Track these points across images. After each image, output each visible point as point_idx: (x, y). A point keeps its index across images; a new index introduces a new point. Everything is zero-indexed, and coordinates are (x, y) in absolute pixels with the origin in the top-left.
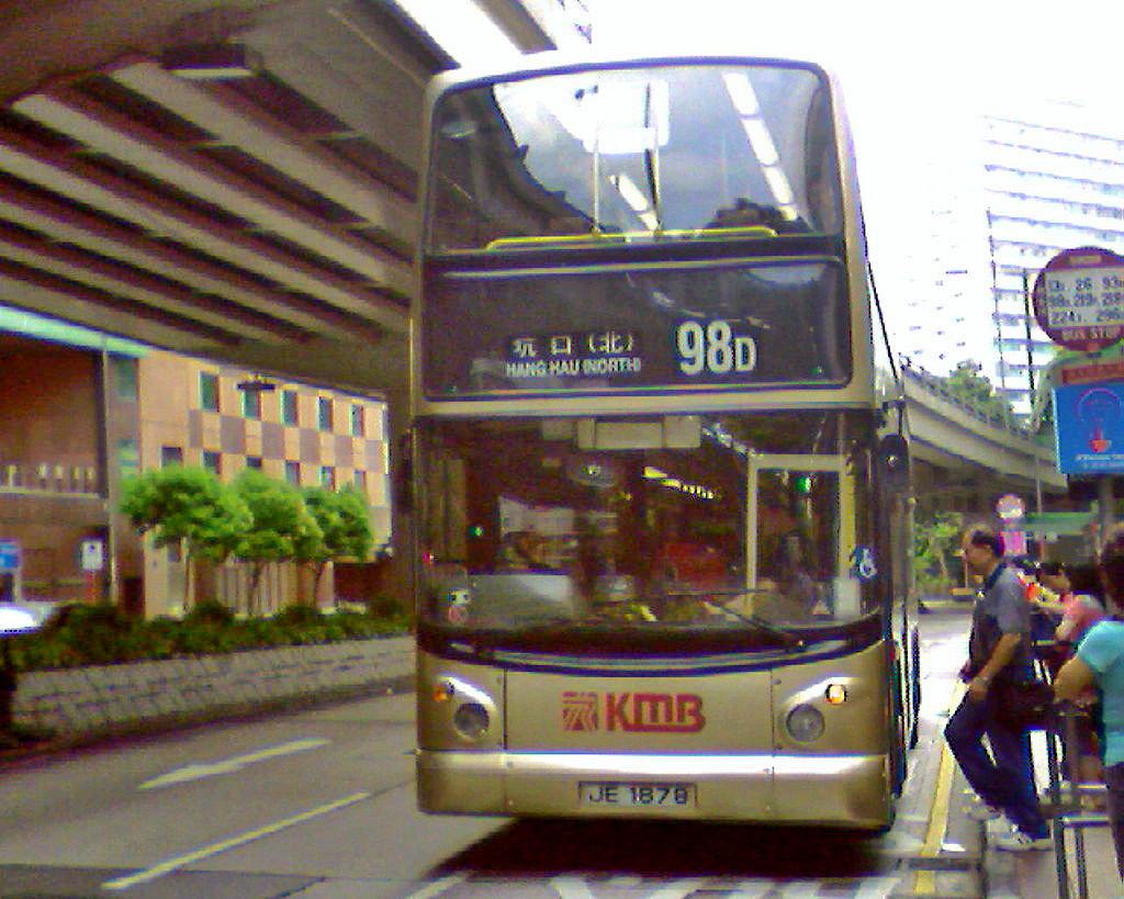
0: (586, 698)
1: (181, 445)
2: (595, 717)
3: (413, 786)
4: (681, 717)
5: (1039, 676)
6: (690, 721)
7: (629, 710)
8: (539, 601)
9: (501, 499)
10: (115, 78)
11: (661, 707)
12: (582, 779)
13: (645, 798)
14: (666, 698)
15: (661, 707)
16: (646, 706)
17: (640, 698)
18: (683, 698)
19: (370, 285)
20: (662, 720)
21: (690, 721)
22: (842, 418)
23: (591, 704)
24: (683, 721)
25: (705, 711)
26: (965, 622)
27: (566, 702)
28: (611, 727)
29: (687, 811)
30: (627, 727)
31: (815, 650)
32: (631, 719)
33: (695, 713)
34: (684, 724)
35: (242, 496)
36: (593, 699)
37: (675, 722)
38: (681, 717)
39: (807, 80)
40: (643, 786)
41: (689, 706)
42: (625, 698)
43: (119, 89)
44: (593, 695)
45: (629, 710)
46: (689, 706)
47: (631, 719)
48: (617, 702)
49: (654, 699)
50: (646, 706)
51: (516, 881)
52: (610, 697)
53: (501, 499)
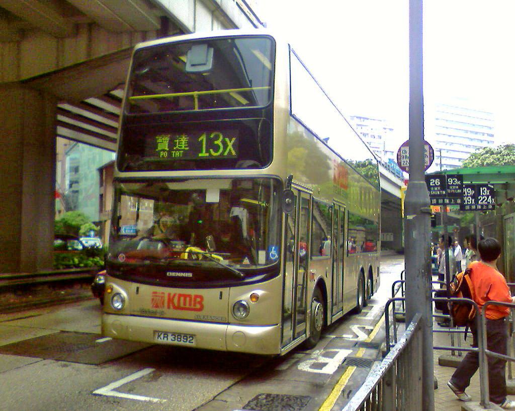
0: (160, 295)
1: (439, 366)
2: (163, 303)
4: (195, 305)
5: (293, 251)
6: (198, 306)
8: (333, 335)
12: (155, 329)
13: (179, 340)
14: (189, 296)
15: (188, 299)
16: (182, 299)
17: (180, 295)
18: (196, 296)
22: (272, 181)
23: (162, 297)
25: (204, 303)
26: (402, 260)
27: (153, 296)
28: (169, 307)
29: (193, 344)
30: (175, 308)
32: (176, 305)
33: (200, 303)
34: (197, 311)
35: (382, 361)
37: (192, 307)
38: (195, 305)
40: (177, 335)
41: (198, 300)
42: (174, 295)
43: (111, 94)
46: (198, 300)
47: (176, 305)
48: (172, 295)
49: (185, 296)
50: (182, 299)
51: (66, 307)
52: (169, 294)
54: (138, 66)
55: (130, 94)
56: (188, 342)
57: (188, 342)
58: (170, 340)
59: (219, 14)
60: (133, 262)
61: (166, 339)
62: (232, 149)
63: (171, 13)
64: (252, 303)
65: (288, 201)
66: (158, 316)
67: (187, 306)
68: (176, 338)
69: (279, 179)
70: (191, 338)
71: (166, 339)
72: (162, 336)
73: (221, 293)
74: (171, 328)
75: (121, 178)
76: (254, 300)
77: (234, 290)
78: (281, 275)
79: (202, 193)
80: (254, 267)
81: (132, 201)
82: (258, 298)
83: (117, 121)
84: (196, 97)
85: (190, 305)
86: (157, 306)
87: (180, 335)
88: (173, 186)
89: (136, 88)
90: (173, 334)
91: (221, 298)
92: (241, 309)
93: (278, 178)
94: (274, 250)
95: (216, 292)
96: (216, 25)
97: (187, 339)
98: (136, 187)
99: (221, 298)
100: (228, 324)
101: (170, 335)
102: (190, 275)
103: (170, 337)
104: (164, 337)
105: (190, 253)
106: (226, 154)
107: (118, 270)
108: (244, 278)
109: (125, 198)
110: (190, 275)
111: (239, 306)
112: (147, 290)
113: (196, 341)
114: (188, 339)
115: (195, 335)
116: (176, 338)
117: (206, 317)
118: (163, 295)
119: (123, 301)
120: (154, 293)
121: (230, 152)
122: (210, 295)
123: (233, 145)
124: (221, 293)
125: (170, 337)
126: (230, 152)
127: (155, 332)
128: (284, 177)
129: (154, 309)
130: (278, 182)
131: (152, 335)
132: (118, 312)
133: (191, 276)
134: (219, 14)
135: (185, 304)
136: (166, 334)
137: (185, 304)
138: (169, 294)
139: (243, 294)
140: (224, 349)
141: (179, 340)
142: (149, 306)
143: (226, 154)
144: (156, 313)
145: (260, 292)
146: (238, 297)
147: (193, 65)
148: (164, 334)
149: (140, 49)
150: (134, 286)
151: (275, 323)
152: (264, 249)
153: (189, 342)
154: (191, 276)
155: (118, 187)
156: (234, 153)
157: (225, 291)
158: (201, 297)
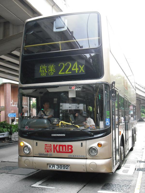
0: (49, 146)
2: (51, 150)
3: (18, 159)
6: (70, 151)
7: (58, 148)
9: (35, 78)
10: (40, 182)
11: (64, 147)
12: (48, 163)
14: (65, 146)
15: (64, 147)
16: (61, 147)
17: (60, 146)
18: (68, 146)
19: (6, 60)
20: (64, 151)
21: (70, 151)
22: (103, 85)
24: (70, 149)
28: (54, 152)
29: (69, 170)
30: (57, 152)
31: (95, 136)
32: (58, 150)
33: (71, 149)
36: (51, 146)
37: (67, 151)
38: (68, 150)
39: (96, 15)
40: (60, 165)
41: (70, 147)
42: (57, 145)
44: (51, 145)
45: (58, 148)
46: (70, 147)
47: (58, 150)
49: (63, 146)
50: (61, 147)
52: (54, 145)
53: (35, 78)
54: (27, 31)
55: (24, 45)
56: (59, 168)
57: (59, 168)
58: (56, 168)
59: (54, 5)
60: (32, 130)
61: (54, 168)
62: (83, 70)
63: (31, 6)
64: (98, 148)
65: (113, 95)
66: (48, 156)
67: (64, 151)
68: (59, 167)
69: (107, 84)
70: (67, 167)
71: (54, 168)
72: (51, 166)
73: (82, 144)
74: (57, 162)
75: (23, 87)
76: (100, 146)
77: (88, 142)
78: (112, 133)
79: (67, 93)
80: (98, 130)
81: (13, 102)
82: (102, 145)
83: (19, 60)
84: (60, 44)
85: (66, 150)
86: (48, 151)
87: (61, 165)
88: (50, 90)
89: (27, 42)
90: (57, 165)
91: (82, 146)
92: (93, 151)
93: (107, 83)
94: (108, 120)
95: (79, 143)
96: (54, 10)
97: (65, 167)
98: (30, 91)
99: (82, 146)
100: (87, 159)
101: (56, 166)
102: (64, 135)
103: (56, 167)
104: (53, 167)
105: (62, 123)
106: (80, 72)
107: (26, 134)
108: (93, 136)
109: (24, 98)
110: (64, 135)
111: (92, 150)
112: (42, 144)
113: (70, 168)
114: (66, 167)
115: (69, 165)
116: (59, 167)
117: (74, 156)
118: (51, 146)
119: (29, 149)
120: (45, 145)
121: (82, 71)
122: (76, 144)
123: (83, 69)
124: (82, 144)
125: (56, 167)
126: (82, 71)
127: (48, 164)
128: (110, 83)
129: (46, 153)
130: (107, 85)
131: (47, 165)
132: (28, 155)
133: (65, 135)
134: (54, 5)
135: (63, 150)
136: (54, 165)
137: (63, 150)
138: (54, 145)
139: (94, 144)
140: (85, 171)
141: (64, 168)
142: (43, 151)
143: (80, 72)
144: (47, 155)
145: (102, 142)
146: (91, 146)
147: (57, 28)
148: (53, 165)
149: (28, 22)
150: (35, 142)
151: (109, 157)
152: (102, 120)
153: (66, 169)
154: (65, 135)
155: (21, 92)
156: (83, 71)
157: (84, 142)
158: (71, 146)
